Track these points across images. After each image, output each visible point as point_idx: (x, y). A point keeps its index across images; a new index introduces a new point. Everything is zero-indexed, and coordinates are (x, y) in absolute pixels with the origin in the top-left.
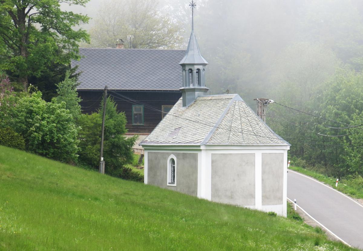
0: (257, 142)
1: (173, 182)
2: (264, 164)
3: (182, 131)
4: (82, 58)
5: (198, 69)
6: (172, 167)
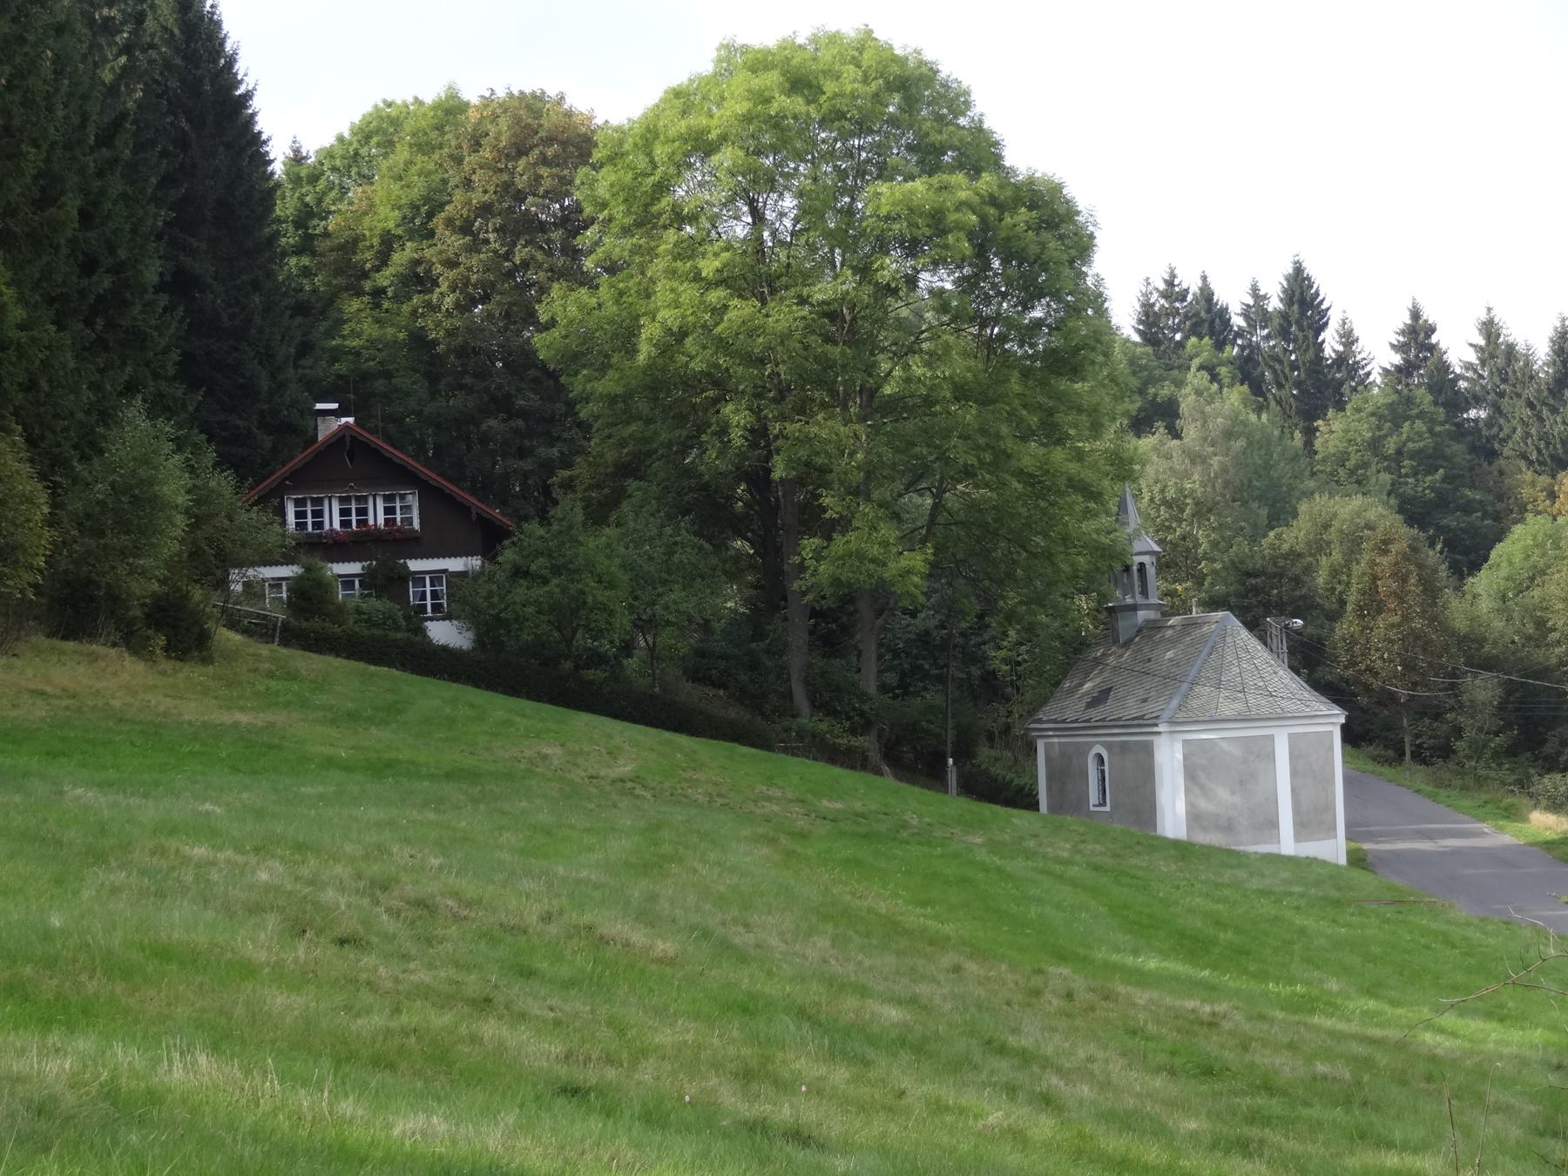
1: (1103, 804)
2: (1294, 757)
4: (674, 607)
5: (1142, 565)
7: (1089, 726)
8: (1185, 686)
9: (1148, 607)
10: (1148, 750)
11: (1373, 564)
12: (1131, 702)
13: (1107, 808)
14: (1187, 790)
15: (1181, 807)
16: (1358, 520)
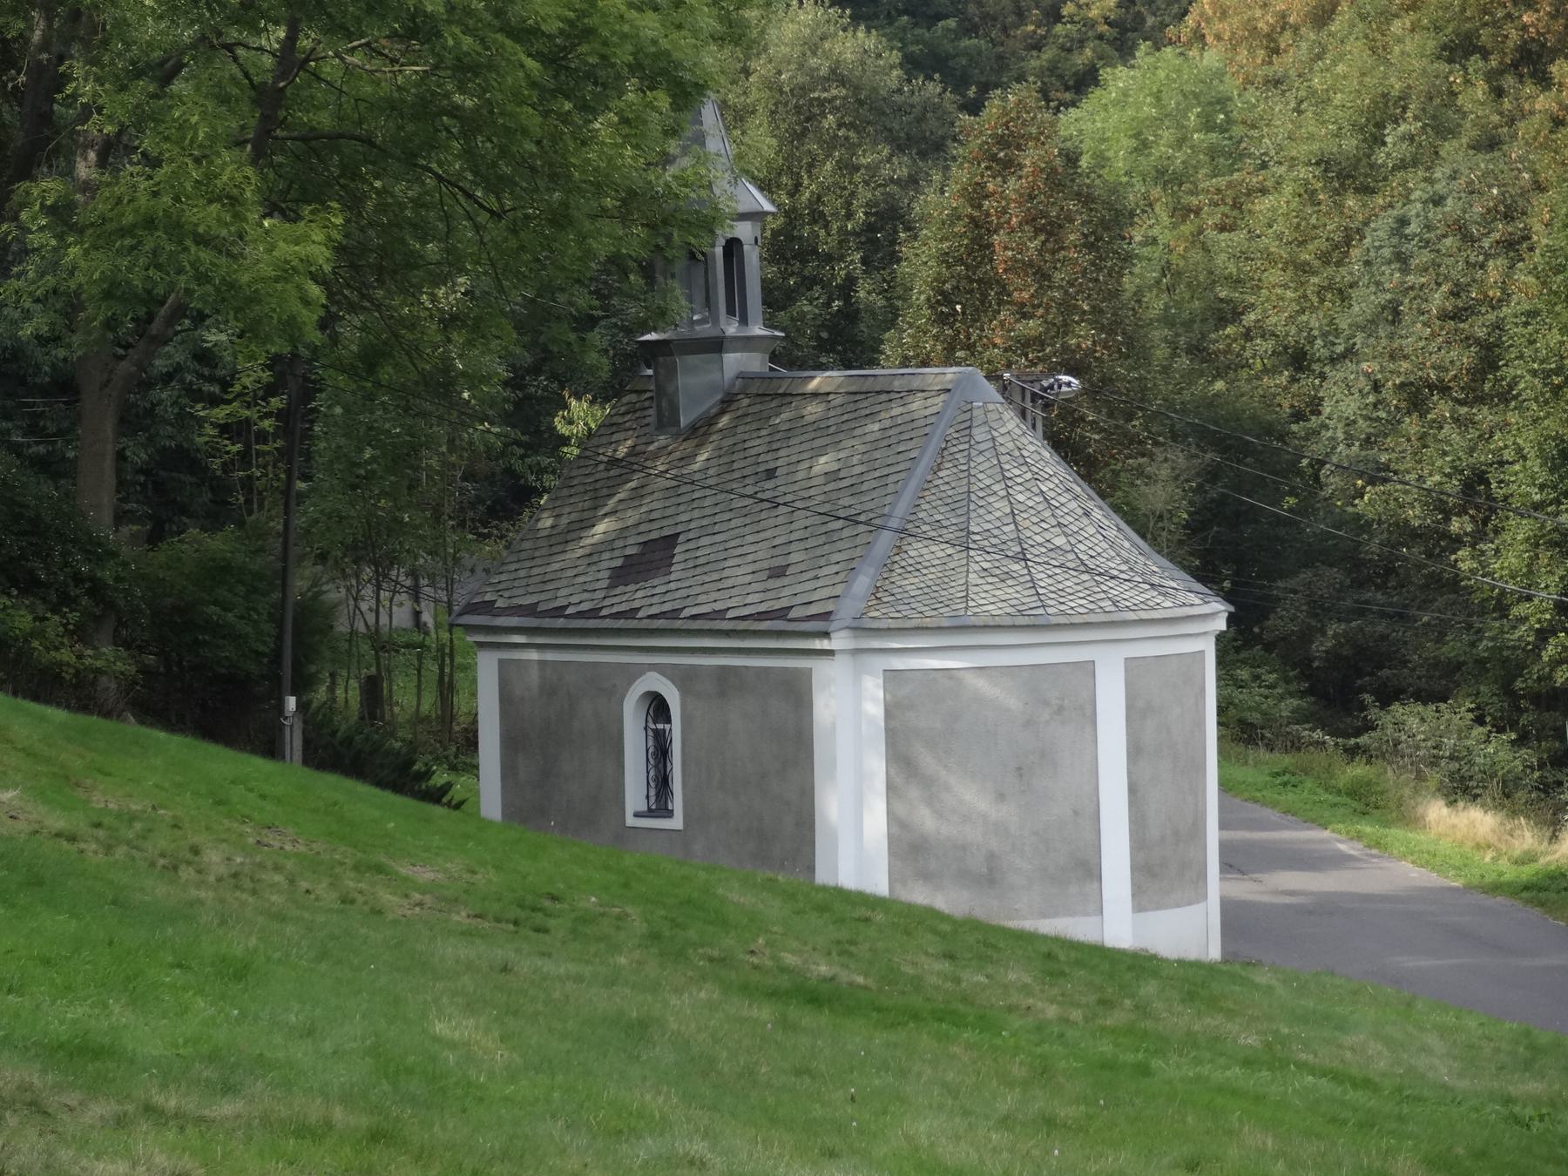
0: (1102, 604)
1: (661, 808)
2: (1137, 712)
3: (688, 555)
6: (650, 733)
7: (627, 626)
8: (885, 539)
9: (748, 343)
10: (797, 692)
11: (976, 195)
12: (739, 574)
13: (676, 822)
14: (891, 788)
15: (876, 821)
16: (813, 62)
